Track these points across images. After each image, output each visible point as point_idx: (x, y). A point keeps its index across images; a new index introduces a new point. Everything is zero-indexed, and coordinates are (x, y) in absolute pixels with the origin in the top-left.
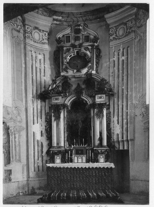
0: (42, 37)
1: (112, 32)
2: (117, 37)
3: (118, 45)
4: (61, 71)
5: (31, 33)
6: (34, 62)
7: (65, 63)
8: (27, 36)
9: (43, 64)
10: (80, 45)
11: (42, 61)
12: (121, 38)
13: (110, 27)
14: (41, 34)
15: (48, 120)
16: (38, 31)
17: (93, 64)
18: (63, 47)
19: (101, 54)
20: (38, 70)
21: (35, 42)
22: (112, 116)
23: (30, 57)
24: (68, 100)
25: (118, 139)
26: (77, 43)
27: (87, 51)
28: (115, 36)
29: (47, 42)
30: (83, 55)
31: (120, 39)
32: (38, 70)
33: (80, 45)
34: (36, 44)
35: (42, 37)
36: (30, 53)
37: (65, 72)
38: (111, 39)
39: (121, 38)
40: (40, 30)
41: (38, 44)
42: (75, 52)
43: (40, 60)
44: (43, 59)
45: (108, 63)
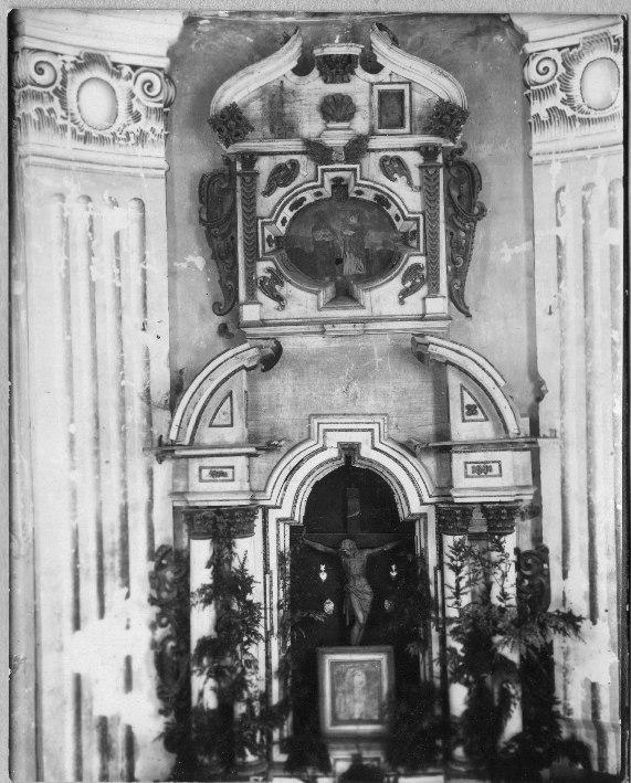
0: (131, 106)
1: (540, 79)
2: (573, 108)
3: (580, 153)
4: (242, 296)
5: (61, 94)
6: (80, 257)
7: (268, 248)
8: (35, 116)
9: (134, 258)
10: (357, 149)
11: (131, 242)
12: (600, 120)
13: (529, 48)
14: (121, 86)
15: (164, 595)
16: (105, 76)
17: (432, 255)
18: (250, 159)
19: (481, 197)
20: (106, 298)
21: (86, 138)
22: (555, 567)
23: (56, 232)
24: (287, 472)
25: (596, 714)
26: (337, 138)
27: (394, 180)
28: (563, 102)
29: (159, 127)
30: (369, 196)
31: (588, 122)
32: (106, 298)
33: (357, 149)
34: (92, 151)
35: (131, 106)
36: (55, 206)
37: (271, 304)
38: (538, 116)
39: (600, 120)
40: (115, 64)
41: (106, 148)
42: (322, 186)
43: (117, 236)
44: (135, 228)
45: (524, 247)
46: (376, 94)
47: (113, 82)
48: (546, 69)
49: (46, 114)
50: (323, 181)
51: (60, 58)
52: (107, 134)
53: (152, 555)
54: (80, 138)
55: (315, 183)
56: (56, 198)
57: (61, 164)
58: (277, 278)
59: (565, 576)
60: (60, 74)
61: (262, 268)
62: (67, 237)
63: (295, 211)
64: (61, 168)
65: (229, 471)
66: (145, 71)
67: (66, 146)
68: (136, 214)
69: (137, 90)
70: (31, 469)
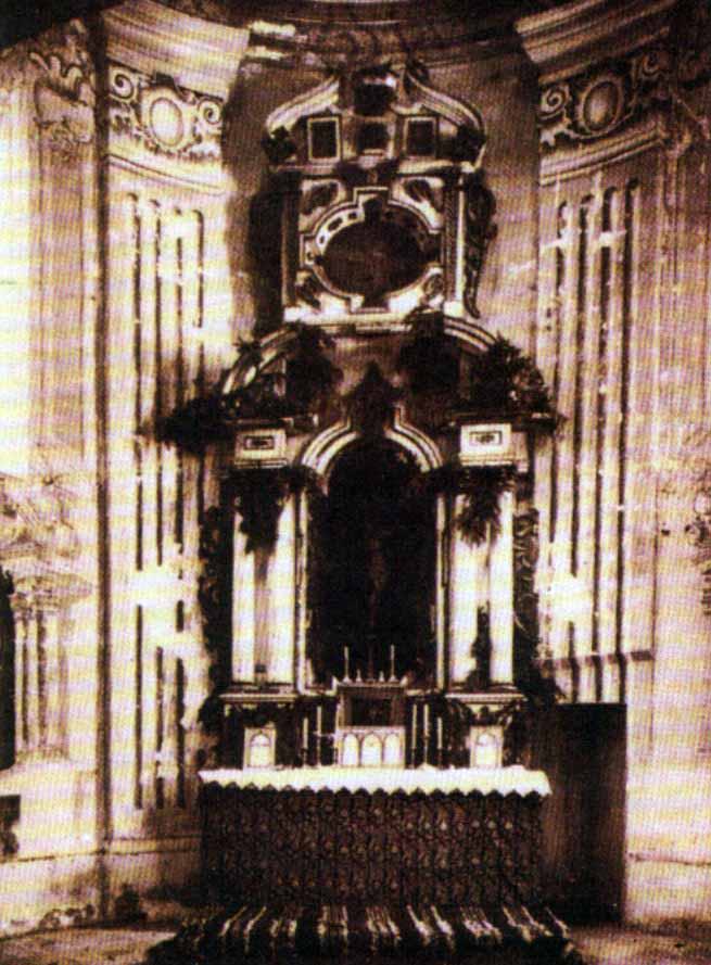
0: (194, 129)
8: (114, 121)
10: (388, 172)
14: (189, 111)
17: (449, 267)
21: (157, 150)
23: (130, 227)
33: (388, 172)
34: (158, 162)
35: (194, 129)
36: (128, 204)
43: (179, 242)
45: (529, 264)
46: (406, 129)
47: (179, 103)
48: (556, 100)
49: (124, 122)
50: (357, 201)
51: (137, 76)
52: (173, 150)
53: (200, 520)
54: (151, 149)
55: (348, 204)
56: (130, 198)
57: (136, 170)
58: (318, 288)
59: (552, 539)
60: (136, 91)
61: (301, 277)
62: (139, 232)
63: (334, 232)
64: (136, 173)
65: (269, 441)
66: (206, 100)
67: (139, 154)
68: (196, 224)
69: (200, 115)
70: (154, 171)
